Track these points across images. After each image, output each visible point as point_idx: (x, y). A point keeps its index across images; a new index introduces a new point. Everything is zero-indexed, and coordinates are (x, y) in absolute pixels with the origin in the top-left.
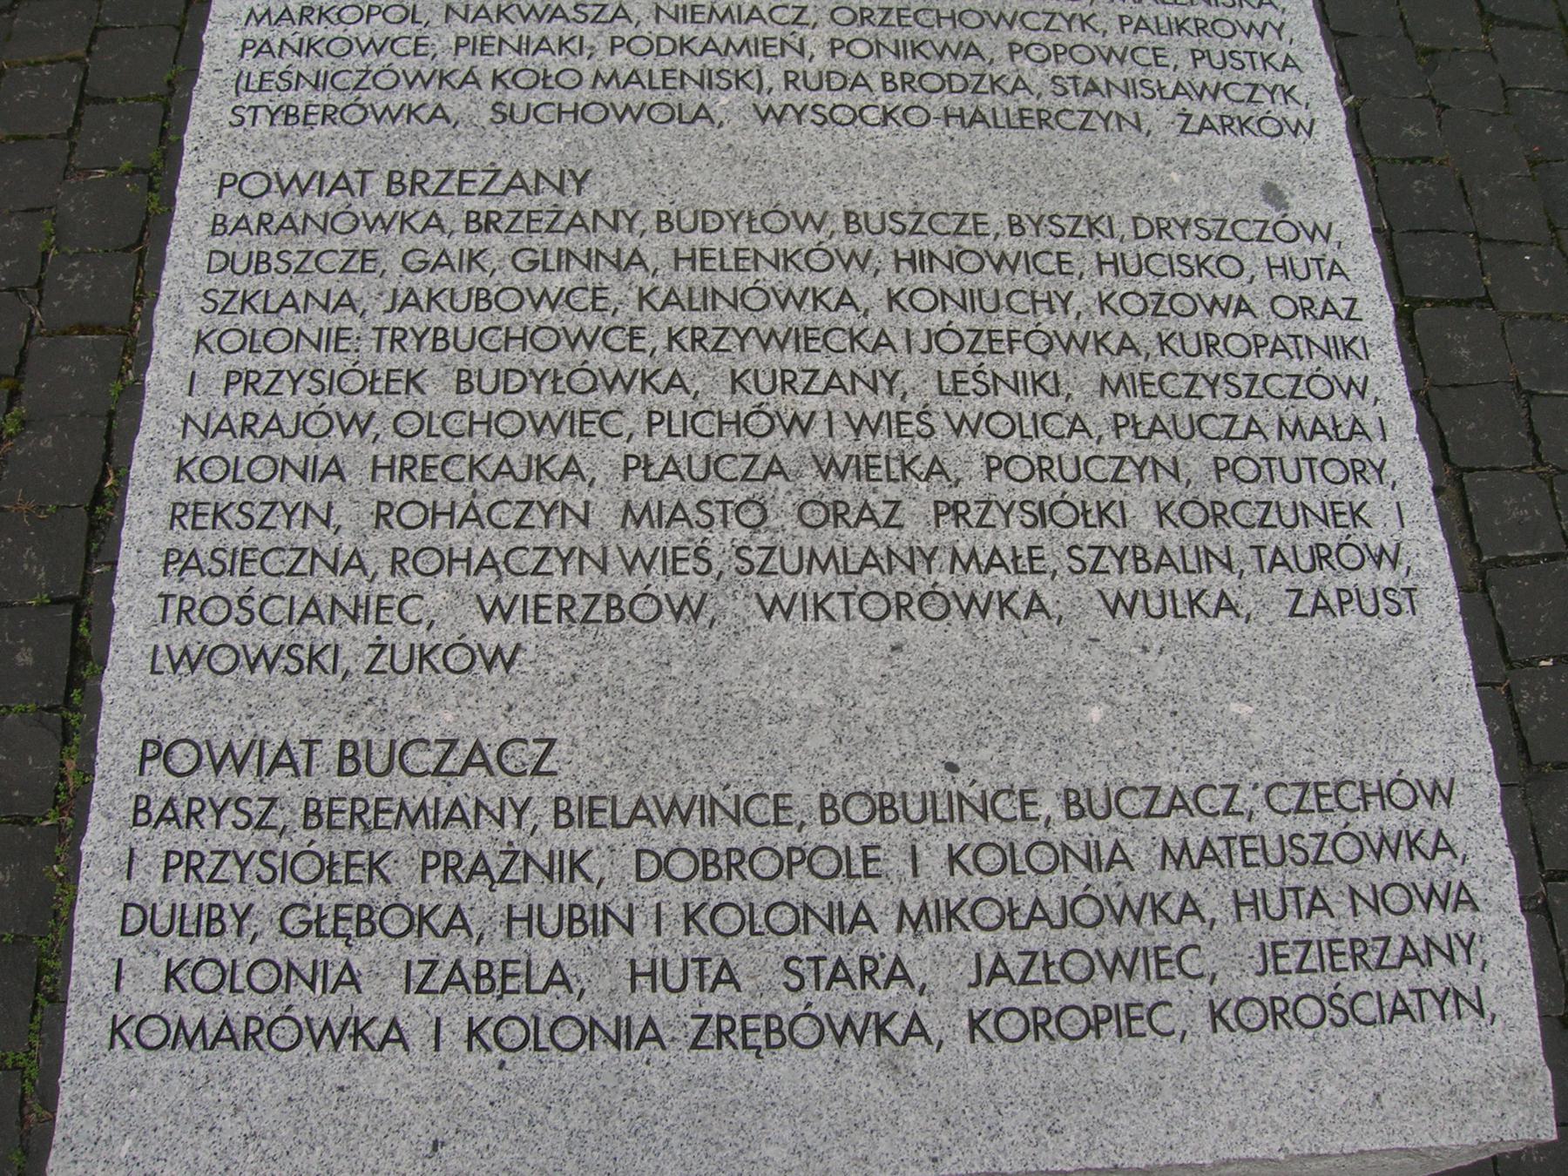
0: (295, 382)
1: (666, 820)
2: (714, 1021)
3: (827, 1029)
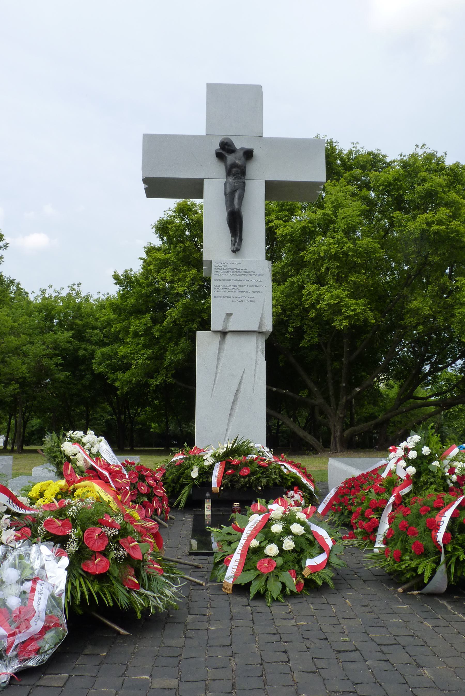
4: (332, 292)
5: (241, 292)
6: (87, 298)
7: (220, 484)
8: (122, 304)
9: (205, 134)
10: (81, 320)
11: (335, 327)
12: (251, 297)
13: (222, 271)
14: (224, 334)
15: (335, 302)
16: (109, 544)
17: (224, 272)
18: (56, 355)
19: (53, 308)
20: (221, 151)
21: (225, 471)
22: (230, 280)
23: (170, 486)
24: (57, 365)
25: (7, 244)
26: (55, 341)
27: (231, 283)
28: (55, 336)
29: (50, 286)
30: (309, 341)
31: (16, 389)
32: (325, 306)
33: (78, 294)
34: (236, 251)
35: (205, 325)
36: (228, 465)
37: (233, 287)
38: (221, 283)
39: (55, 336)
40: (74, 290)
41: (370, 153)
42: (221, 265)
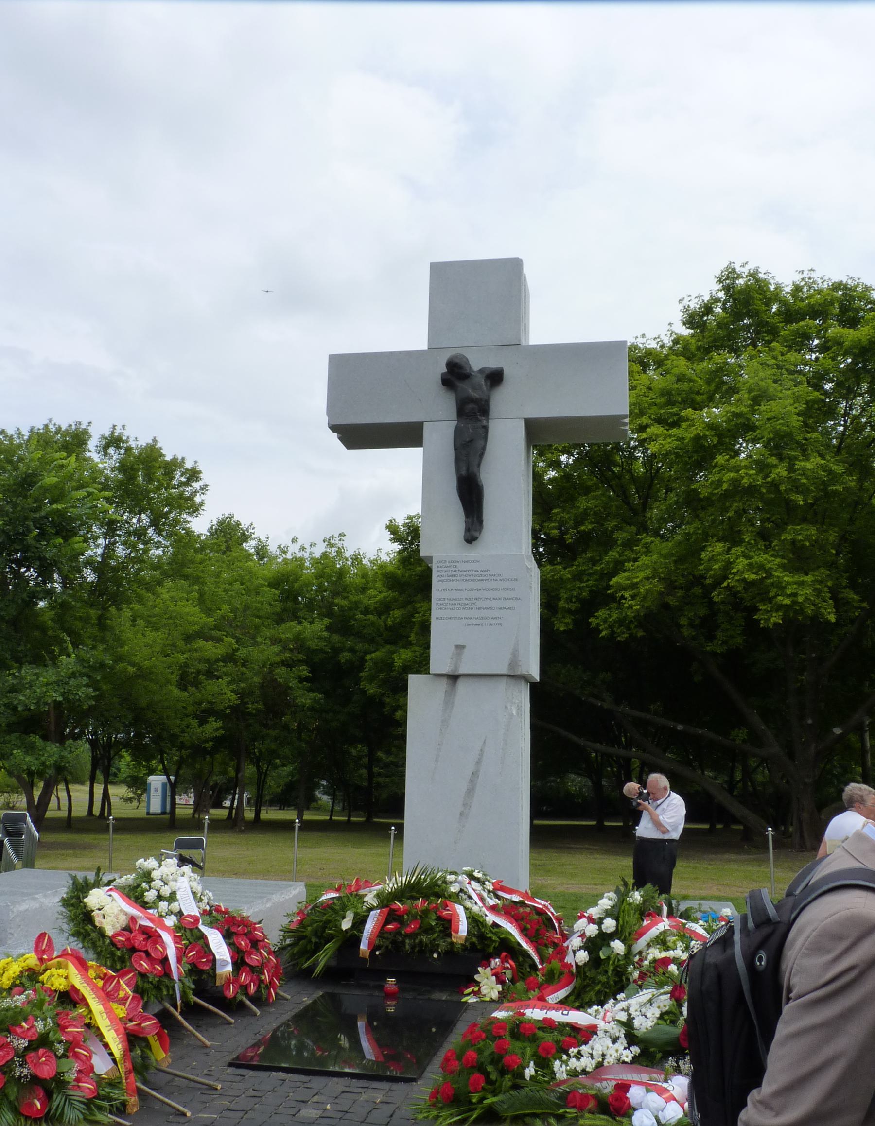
4: (752, 557)
5: (479, 609)
6: (356, 558)
7: (373, 948)
8: (403, 576)
9: (425, 347)
10: (345, 598)
11: (758, 621)
12: (496, 618)
13: (450, 574)
14: (454, 678)
15: (753, 577)
16: (13, 1058)
17: (452, 576)
18: (301, 662)
19: (296, 580)
20: (449, 377)
21: (387, 922)
22: (462, 590)
23: (310, 941)
24: (301, 680)
25: (207, 486)
26: (298, 638)
27: (464, 595)
28: (299, 628)
29: (294, 540)
30: (725, 642)
31: (217, 730)
32: (737, 584)
33: (339, 553)
34: (471, 538)
35: (422, 665)
36: (392, 916)
37: (467, 602)
38: (446, 595)
39: (299, 628)
40: (332, 545)
41: (837, 286)
42: (447, 564)
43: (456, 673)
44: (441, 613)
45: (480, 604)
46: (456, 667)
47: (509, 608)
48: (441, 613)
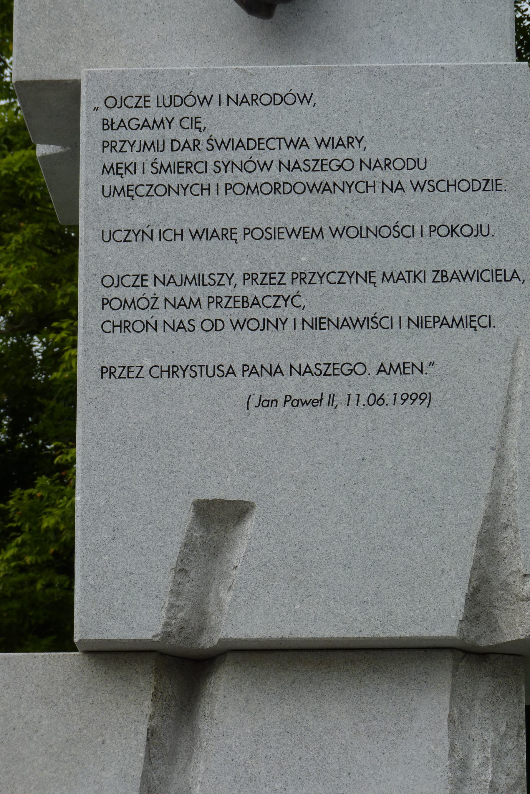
0: (184, 371)
1: (464, 279)
2: (440, 272)
3: (257, 166)
5: (316, 324)
13: (166, 158)
14: (182, 671)
17: (175, 168)
22: (227, 234)
37: (251, 291)
42: (153, 113)
43: (207, 642)
44: (127, 349)
45: (316, 300)
46: (201, 621)
47: (467, 322)
48: (127, 349)
